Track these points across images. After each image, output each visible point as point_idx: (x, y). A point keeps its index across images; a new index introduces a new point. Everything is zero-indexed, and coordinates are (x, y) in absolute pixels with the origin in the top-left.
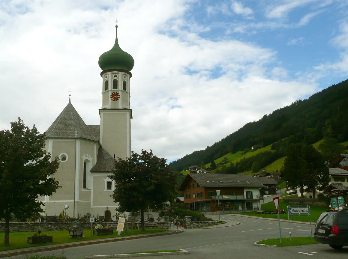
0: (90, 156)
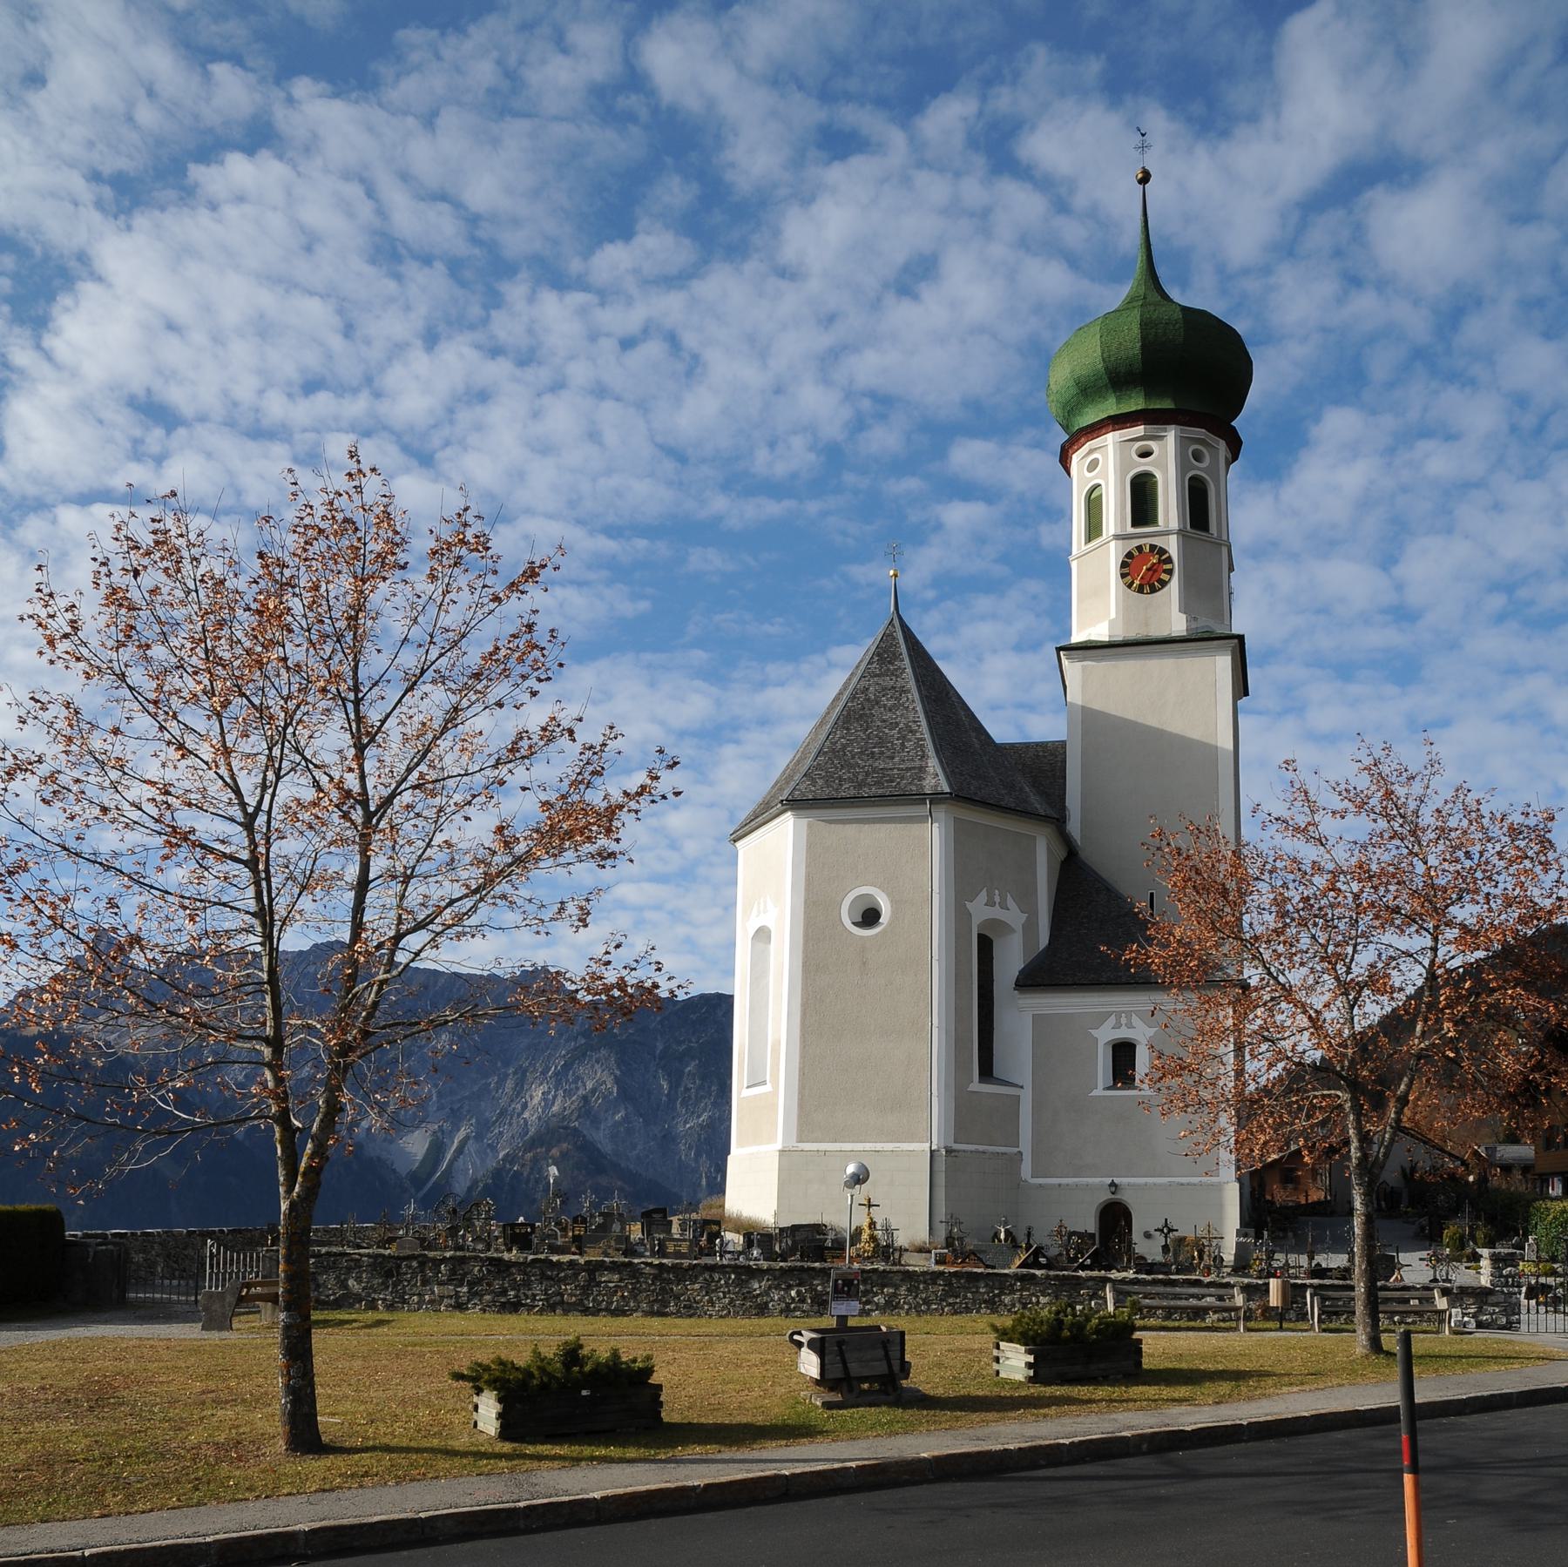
0: (1010, 902)
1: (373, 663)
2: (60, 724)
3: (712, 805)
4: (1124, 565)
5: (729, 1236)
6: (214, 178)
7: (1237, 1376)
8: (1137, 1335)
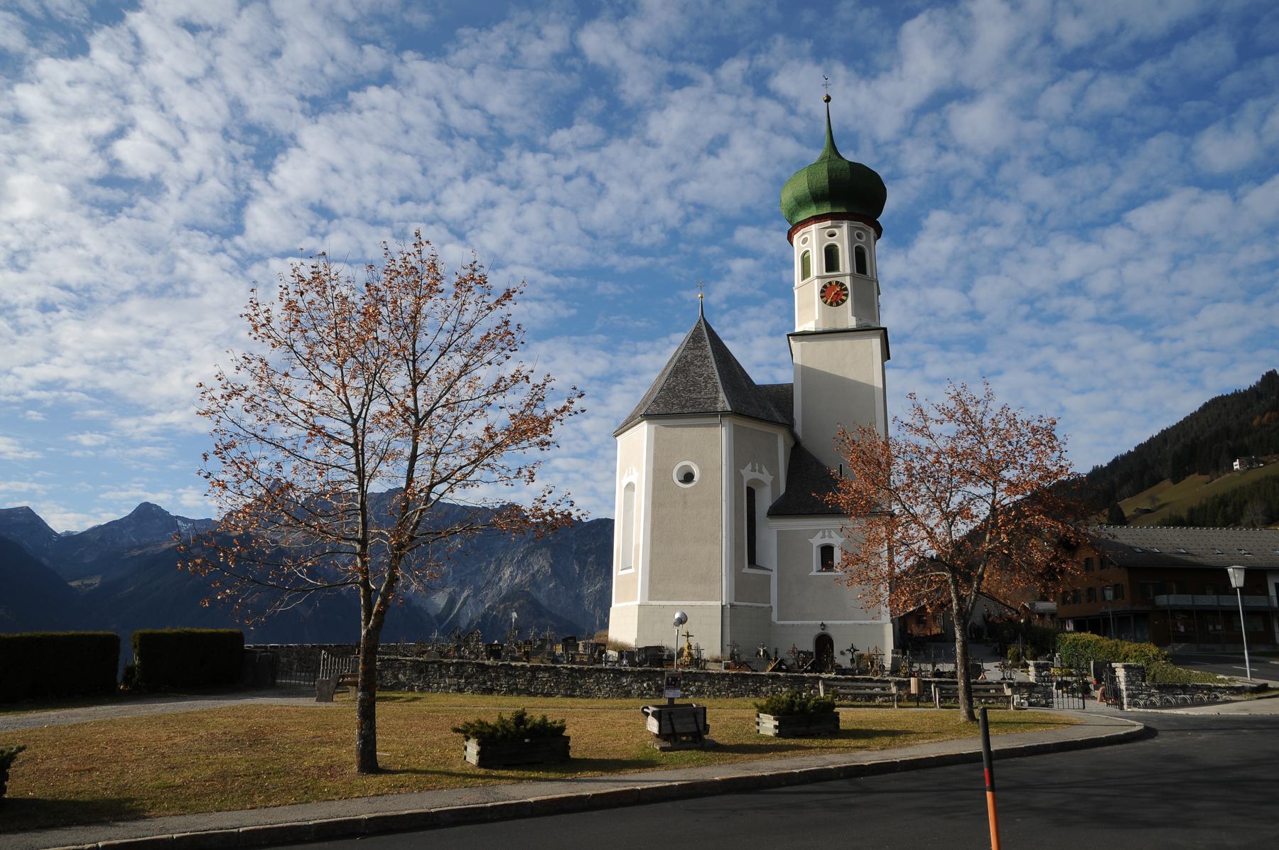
0: (764, 469)
1: (423, 341)
2: (258, 371)
3: (606, 417)
4: (822, 291)
5: (610, 652)
6: (358, 98)
7: (893, 734)
8: (836, 710)
